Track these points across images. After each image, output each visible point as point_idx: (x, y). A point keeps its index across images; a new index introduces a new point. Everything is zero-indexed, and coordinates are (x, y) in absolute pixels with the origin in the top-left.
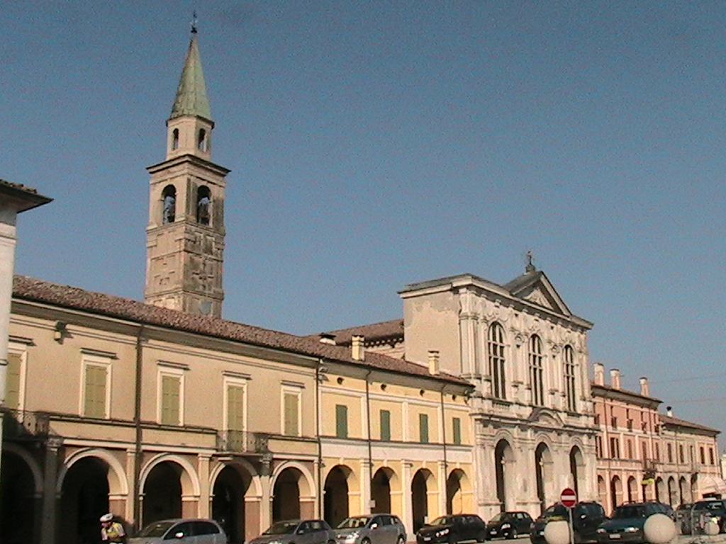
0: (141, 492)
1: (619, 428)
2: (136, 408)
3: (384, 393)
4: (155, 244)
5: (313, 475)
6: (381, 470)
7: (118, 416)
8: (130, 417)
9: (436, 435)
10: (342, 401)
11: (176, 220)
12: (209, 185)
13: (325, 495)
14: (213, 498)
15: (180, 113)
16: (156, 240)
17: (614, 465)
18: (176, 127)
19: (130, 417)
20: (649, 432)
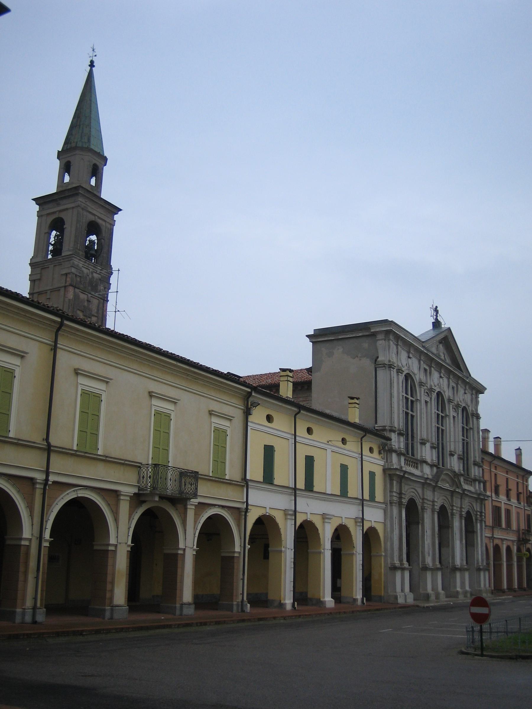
0: (47, 535)
1: (501, 496)
2: (27, 441)
3: (309, 437)
4: (39, 278)
5: (31, 515)
6: (260, 522)
7: (25, 436)
8: (38, 438)
9: (353, 490)
10: (270, 442)
11: (63, 254)
12: (100, 221)
13: (249, 550)
14: (132, 548)
15: (73, 145)
16: (41, 273)
17: (498, 534)
18: (68, 159)
19: (38, 438)
20: (522, 503)
